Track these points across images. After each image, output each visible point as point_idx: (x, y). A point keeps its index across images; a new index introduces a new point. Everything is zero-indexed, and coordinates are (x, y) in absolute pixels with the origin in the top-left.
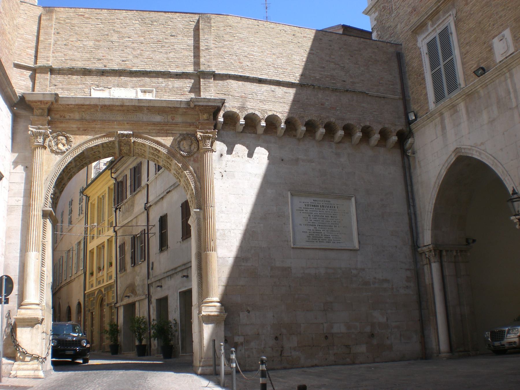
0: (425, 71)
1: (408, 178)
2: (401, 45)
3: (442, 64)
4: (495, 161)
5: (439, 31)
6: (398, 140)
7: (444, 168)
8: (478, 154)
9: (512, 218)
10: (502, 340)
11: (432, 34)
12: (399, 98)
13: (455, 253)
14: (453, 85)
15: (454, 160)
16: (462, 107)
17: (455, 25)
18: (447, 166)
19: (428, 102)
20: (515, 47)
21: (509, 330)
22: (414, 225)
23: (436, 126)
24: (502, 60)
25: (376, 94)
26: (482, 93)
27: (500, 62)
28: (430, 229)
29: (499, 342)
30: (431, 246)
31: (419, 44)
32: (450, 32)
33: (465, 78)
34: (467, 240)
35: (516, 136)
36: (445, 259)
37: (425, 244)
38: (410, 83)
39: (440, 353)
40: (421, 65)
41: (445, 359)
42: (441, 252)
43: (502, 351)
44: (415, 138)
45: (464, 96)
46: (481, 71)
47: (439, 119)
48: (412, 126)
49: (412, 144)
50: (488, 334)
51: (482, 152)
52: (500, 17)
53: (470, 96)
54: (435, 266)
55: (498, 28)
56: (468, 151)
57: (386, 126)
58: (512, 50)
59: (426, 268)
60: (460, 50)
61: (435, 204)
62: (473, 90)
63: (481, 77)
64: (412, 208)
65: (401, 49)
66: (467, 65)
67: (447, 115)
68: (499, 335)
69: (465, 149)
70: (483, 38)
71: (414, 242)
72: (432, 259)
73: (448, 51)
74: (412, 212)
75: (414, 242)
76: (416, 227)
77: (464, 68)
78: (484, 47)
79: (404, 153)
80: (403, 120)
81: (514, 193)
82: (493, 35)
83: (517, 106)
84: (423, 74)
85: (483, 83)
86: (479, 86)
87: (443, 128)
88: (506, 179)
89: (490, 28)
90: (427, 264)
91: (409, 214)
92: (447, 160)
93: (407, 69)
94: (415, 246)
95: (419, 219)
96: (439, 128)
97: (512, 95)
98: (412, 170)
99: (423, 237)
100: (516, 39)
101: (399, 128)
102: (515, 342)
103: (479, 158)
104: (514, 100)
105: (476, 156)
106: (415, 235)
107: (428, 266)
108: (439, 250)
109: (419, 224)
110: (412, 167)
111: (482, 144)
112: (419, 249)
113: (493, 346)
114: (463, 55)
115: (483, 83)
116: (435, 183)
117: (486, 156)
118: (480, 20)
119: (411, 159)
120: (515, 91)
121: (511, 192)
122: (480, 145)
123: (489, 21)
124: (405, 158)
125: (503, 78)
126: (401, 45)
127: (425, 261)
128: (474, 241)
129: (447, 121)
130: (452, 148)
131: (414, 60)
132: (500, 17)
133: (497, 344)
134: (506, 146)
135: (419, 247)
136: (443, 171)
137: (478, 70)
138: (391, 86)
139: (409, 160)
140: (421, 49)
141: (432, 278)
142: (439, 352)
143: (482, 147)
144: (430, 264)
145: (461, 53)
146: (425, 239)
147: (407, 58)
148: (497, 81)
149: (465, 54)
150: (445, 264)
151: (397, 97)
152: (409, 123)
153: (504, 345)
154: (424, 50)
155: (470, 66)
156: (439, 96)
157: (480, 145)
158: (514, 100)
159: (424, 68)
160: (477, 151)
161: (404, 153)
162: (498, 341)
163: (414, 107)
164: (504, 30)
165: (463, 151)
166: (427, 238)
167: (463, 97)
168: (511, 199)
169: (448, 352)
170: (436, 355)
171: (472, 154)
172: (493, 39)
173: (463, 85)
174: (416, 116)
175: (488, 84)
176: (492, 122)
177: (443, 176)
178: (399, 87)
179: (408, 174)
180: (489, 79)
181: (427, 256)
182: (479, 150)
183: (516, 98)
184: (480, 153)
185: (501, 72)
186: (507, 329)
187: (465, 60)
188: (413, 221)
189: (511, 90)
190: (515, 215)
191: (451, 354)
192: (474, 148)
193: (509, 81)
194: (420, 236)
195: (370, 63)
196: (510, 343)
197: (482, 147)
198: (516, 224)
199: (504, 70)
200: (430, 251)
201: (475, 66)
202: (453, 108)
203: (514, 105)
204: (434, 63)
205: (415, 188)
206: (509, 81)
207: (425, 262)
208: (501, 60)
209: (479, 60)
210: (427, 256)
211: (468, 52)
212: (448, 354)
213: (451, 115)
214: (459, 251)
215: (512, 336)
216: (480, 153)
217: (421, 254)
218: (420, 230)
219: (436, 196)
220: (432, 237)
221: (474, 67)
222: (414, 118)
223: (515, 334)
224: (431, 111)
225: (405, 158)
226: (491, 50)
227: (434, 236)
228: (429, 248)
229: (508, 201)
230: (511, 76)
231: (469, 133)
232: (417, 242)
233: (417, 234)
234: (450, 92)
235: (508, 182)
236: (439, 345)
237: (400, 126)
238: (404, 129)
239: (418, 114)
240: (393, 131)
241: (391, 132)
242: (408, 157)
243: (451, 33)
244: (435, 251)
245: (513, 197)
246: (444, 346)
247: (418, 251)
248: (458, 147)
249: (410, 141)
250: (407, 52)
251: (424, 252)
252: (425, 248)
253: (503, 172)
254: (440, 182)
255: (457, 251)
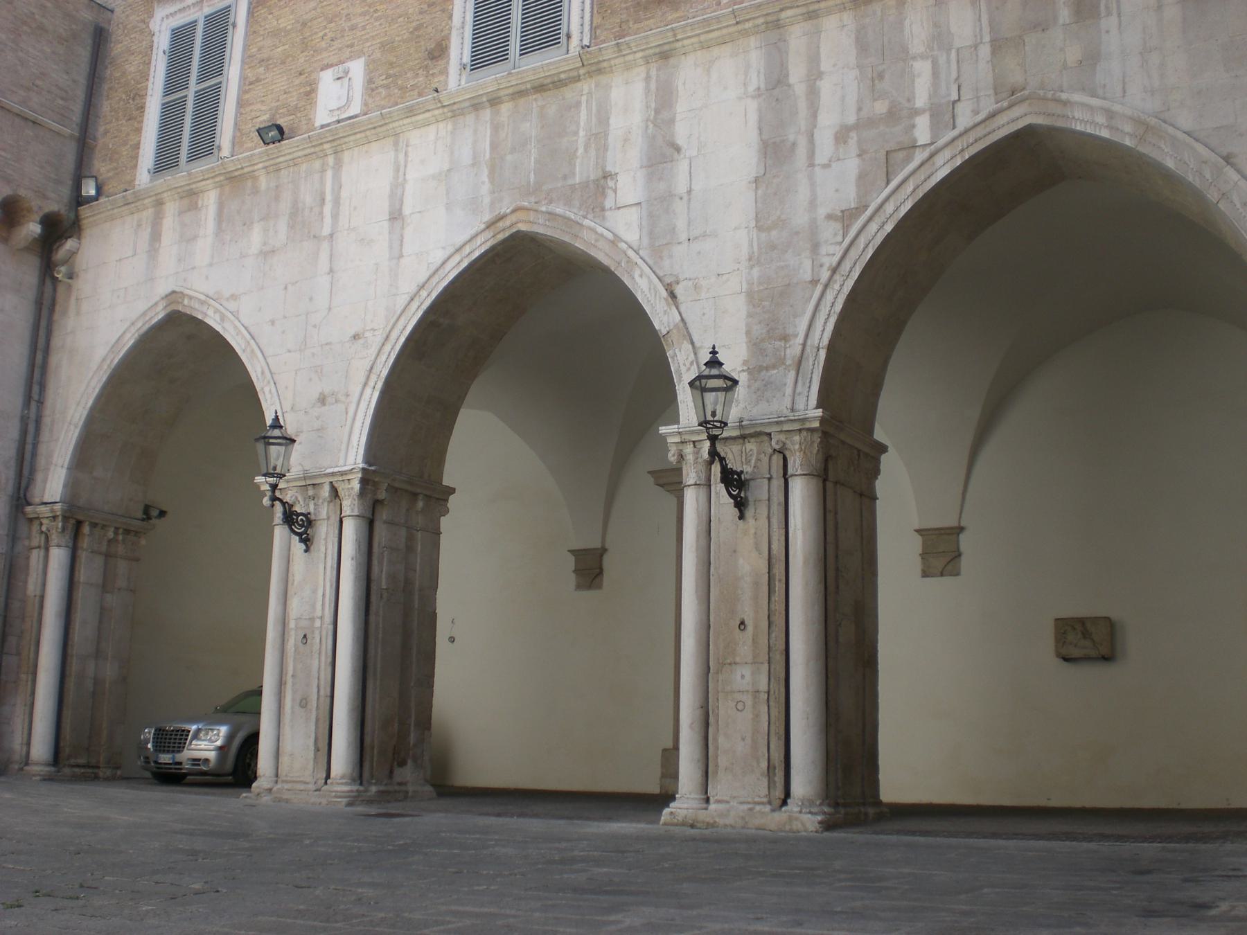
0: (150, 92)
1: (42, 332)
2: (112, 11)
3: (193, 87)
4: (252, 342)
5: (207, 10)
6: (40, 235)
7: (133, 330)
8: (217, 317)
9: (259, 479)
10: (179, 752)
11: (192, 10)
12: (72, 136)
13: (111, 534)
14: (204, 146)
15: (160, 316)
16: (210, 200)
17: (249, 12)
18: (142, 326)
19: (136, 166)
20: (365, 104)
21: (199, 730)
22: (29, 447)
23: (139, 225)
24: (328, 125)
25: (17, 108)
26: (263, 182)
27: (322, 126)
28: (66, 465)
29: (170, 756)
30: (58, 507)
31: (155, 25)
32: (231, 20)
33: (234, 137)
34: (147, 509)
35: (311, 299)
36: (85, 543)
37: (45, 500)
38: (106, 107)
39: (27, 764)
40: (145, 76)
41: (38, 778)
42: (79, 524)
43: (171, 777)
44: (83, 241)
45: (222, 178)
46: (275, 133)
47: (151, 211)
48: (85, 211)
49: (73, 254)
50: (149, 733)
51: (230, 315)
52: (353, 28)
53: (235, 181)
54: (58, 557)
55: (340, 49)
56: (197, 306)
57: (22, 192)
58: (355, 109)
59: (36, 557)
60: (242, 69)
61: (92, 409)
62: (246, 170)
63: (272, 146)
64: (33, 405)
65: (109, 22)
66: (248, 109)
67: (171, 208)
68: (173, 740)
69: (191, 298)
70: (302, 60)
71: (19, 489)
72: (55, 538)
73: (214, 63)
74: (33, 415)
75: (19, 489)
76: (34, 454)
77: (239, 114)
78: (297, 82)
79: (48, 268)
80: (66, 191)
81: (276, 424)
82: (325, 62)
83: (331, 235)
84: (143, 96)
85: (272, 162)
86: (260, 166)
87: (156, 236)
88: (267, 390)
89: (323, 44)
90: (39, 547)
91: (24, 421)
92: (144, 314)
93: (108, 72)
94: (21, 499)
95: (45, 436)
96: (146, 233)
97: (328, 209)
98: (56, 317)
99: (45, 481)
100: (371, 87)
101: (52, 207)
102: (207, 760)
103: (218, 328)
104: (328, 220)
105: (212, 321)
106: (26, 472)
107: (42, 552)
108: (75, 521)
109: (42, 449)
110: (57, 308)
111: (234, 297)
112: (29, 509)
113: (156, 762)
114: (247, 84)
115: (272, 162)
116: (104, 360)
117: (235, 327)
118: (305, 17)
119: (61, 289)
120: (337, 202)
121: (269, 422)
122: (227, 299)
123: (325, 27)
124: (48, 282)
125: (317, 164)
126: (112, 11)
127: (37, 540)
128: (162, 514)
129: (170, 222)
130: (163, 288)
131: (132, 58)
132: (353, 28)
133: (165, 758)
134: (285, 317)
135: (29, 504)
136: (128, 335)
137: (269, 128)
138: (61, 102)
139: (55, 290)
140: (155, 39)
141: (44, 584)
142: (27, 760)
143: (232, 306)
144: (47, 549)
145: (243, 78)
146: (48, 486)
147: (117, 48)
148: (304, 167)
149: (251, 84)
150: (83, 556)
151: (67, 131)
152: (79, 201)
153: (180, 763)
154: (163, 42)
155: (253, 114)
156: (166, 161)
157: (227, 299)
158: (328, 220)
159: (151, 79)
160: (216, 311)
161: (48, 268)
162: (168, 752)
163: (101, 166)
164: (351, 58)
165: (186, 302)
166: (53, 485)
167: (217, 179)
168: (265, 438)
169: (49, 765)
170: (16, 767)
171: (206, 314)
172: (322, 70)
173: (225, 152)
174: (99, 189)
175: (282, 166)
176: (267, 253)
177: (126, 349)
178: (77, 108)
179: (43, 323)
180: (288, 157)
181: (44, 528)
182: (221, 308)
183: (335, 216)
184: (223, 318)
185: (317, 149)
186: (194, 727)
187: (247, 96)
188: (30, 439)
189: (329, 197)
190: (265, 475)
191: (53, 769)
192: (212, 302)
193: (329, 174)
194: (39, 477)
195: (25, 28)
196: (195, 760)
197: (232, 306)
198: (263, 494)
199: (326, 146)
200: (54, 517)
201: (265, 117)
202: (191, 196)
203: (326, 231)
204: (176, 80)
205: (53, 360)
206: (329, 174)
207: (35, 543)
208: (325, 122)
209: (277, 108)
210: (44, 528)
211: (258, 80)
212: (47, 769)
213: (181, 213)
214: (121, 531)
215: (203, 744)
216: (223, 318)
217: (31, 520)
218: (41, 461)
219: (97, 390)
220: (65, 486)
221: (264, 119)
222: (93, 192)
223: (210, 741)
224: (137, 188)
225: (48, 282)
226: (310, 92)
227: (72, 485)
228: (52, 511)
229: (257, 440)
230: (338, 165)
231: (211, 265)
232: (27, 488)
233: (33, 470)
234: (193, 158)
235: (268, 396)
236: (29, 744)
237: (56, 203)
238: (63, 211)
239: (106, 188)
240: (35, 209)
241: (30, 210)
242: (55, 280)
243: (234, 26)
244: (65, 518)
245: (269, 434)
246: (40, 748)
247: (24, 513)
248: (177, 289)
249: (70, 244)
250: (120, 32)
251: (38, 518)
252: (42, 509)
253: (263, 373)
254: (116, 361)
255: (117, 529)
